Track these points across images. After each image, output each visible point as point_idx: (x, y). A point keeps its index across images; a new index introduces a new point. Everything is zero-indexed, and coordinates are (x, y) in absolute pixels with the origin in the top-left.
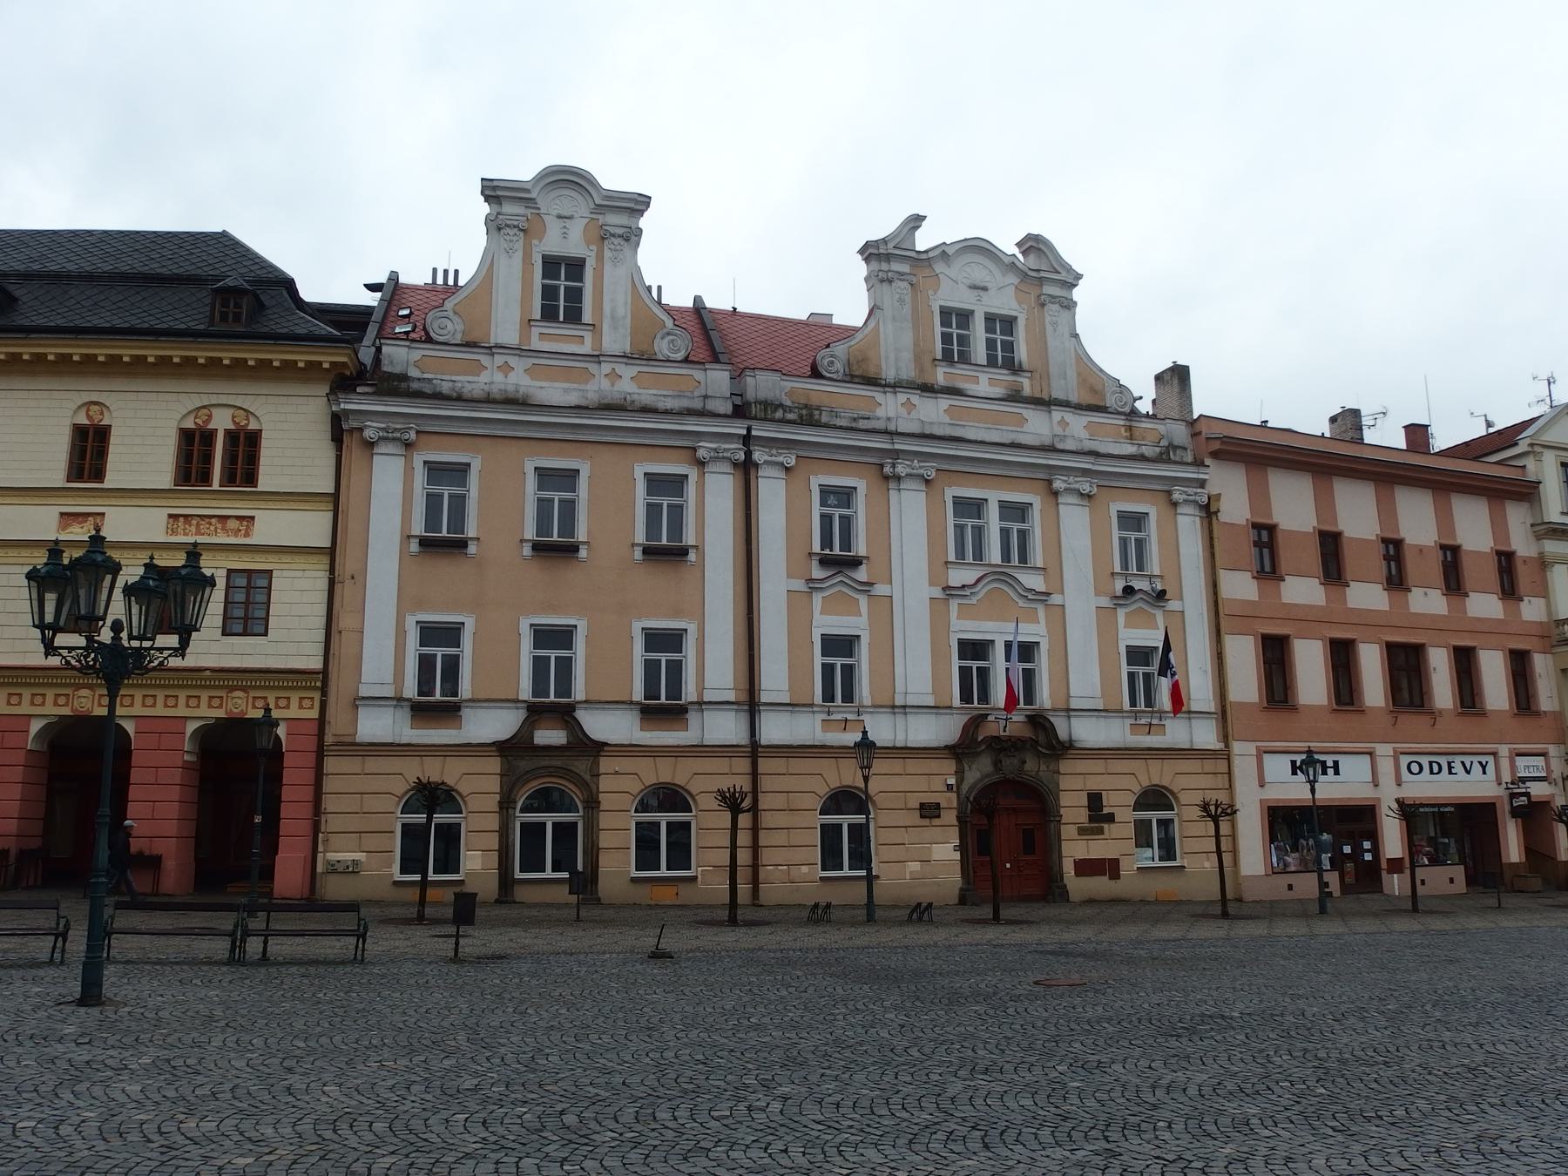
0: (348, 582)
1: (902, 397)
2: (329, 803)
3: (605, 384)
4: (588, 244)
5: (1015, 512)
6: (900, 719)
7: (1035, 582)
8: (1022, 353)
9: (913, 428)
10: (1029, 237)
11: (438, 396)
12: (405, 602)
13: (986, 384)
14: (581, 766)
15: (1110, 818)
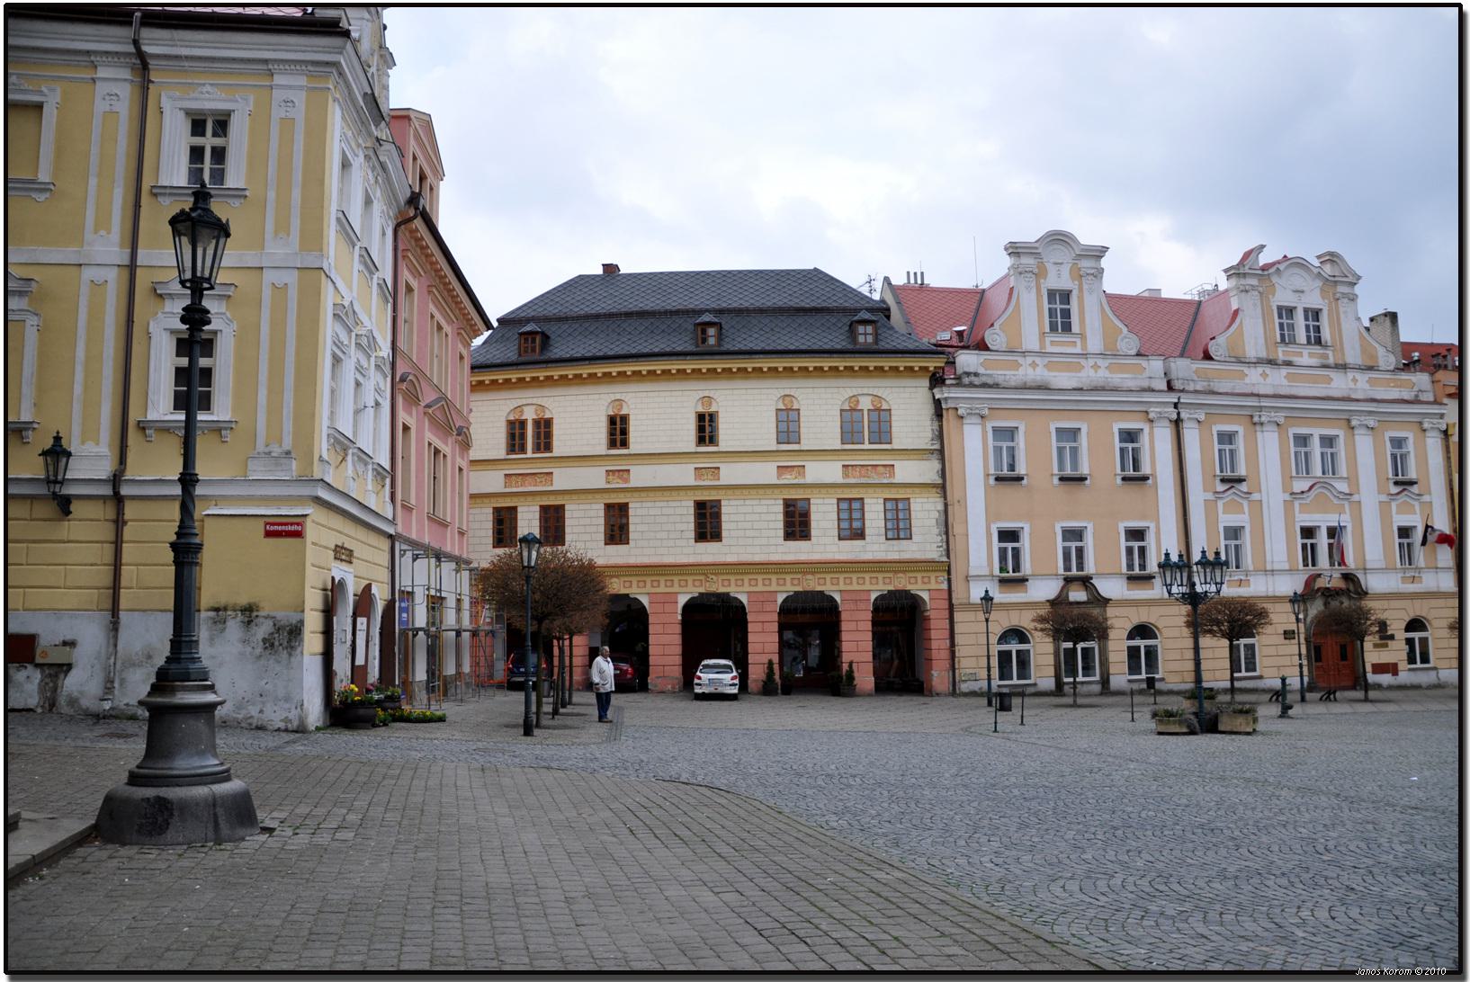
0: (956, 506)
1: (1260, 370)
2: (958, 639)
3: (1092, 373)
4: (1073, 279)
5: (1328, 441)
6: (1270, 578)
7: (1342, 487)
8: (1326, 334)
9: (1270, 391)
10: (1332, 254)
11: (996, 386)
12: (990, 516)
13: (1307, 357)
14: (1096, 612)
15: (1392, 637)
